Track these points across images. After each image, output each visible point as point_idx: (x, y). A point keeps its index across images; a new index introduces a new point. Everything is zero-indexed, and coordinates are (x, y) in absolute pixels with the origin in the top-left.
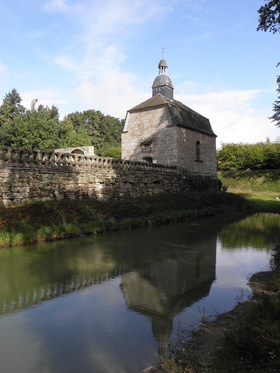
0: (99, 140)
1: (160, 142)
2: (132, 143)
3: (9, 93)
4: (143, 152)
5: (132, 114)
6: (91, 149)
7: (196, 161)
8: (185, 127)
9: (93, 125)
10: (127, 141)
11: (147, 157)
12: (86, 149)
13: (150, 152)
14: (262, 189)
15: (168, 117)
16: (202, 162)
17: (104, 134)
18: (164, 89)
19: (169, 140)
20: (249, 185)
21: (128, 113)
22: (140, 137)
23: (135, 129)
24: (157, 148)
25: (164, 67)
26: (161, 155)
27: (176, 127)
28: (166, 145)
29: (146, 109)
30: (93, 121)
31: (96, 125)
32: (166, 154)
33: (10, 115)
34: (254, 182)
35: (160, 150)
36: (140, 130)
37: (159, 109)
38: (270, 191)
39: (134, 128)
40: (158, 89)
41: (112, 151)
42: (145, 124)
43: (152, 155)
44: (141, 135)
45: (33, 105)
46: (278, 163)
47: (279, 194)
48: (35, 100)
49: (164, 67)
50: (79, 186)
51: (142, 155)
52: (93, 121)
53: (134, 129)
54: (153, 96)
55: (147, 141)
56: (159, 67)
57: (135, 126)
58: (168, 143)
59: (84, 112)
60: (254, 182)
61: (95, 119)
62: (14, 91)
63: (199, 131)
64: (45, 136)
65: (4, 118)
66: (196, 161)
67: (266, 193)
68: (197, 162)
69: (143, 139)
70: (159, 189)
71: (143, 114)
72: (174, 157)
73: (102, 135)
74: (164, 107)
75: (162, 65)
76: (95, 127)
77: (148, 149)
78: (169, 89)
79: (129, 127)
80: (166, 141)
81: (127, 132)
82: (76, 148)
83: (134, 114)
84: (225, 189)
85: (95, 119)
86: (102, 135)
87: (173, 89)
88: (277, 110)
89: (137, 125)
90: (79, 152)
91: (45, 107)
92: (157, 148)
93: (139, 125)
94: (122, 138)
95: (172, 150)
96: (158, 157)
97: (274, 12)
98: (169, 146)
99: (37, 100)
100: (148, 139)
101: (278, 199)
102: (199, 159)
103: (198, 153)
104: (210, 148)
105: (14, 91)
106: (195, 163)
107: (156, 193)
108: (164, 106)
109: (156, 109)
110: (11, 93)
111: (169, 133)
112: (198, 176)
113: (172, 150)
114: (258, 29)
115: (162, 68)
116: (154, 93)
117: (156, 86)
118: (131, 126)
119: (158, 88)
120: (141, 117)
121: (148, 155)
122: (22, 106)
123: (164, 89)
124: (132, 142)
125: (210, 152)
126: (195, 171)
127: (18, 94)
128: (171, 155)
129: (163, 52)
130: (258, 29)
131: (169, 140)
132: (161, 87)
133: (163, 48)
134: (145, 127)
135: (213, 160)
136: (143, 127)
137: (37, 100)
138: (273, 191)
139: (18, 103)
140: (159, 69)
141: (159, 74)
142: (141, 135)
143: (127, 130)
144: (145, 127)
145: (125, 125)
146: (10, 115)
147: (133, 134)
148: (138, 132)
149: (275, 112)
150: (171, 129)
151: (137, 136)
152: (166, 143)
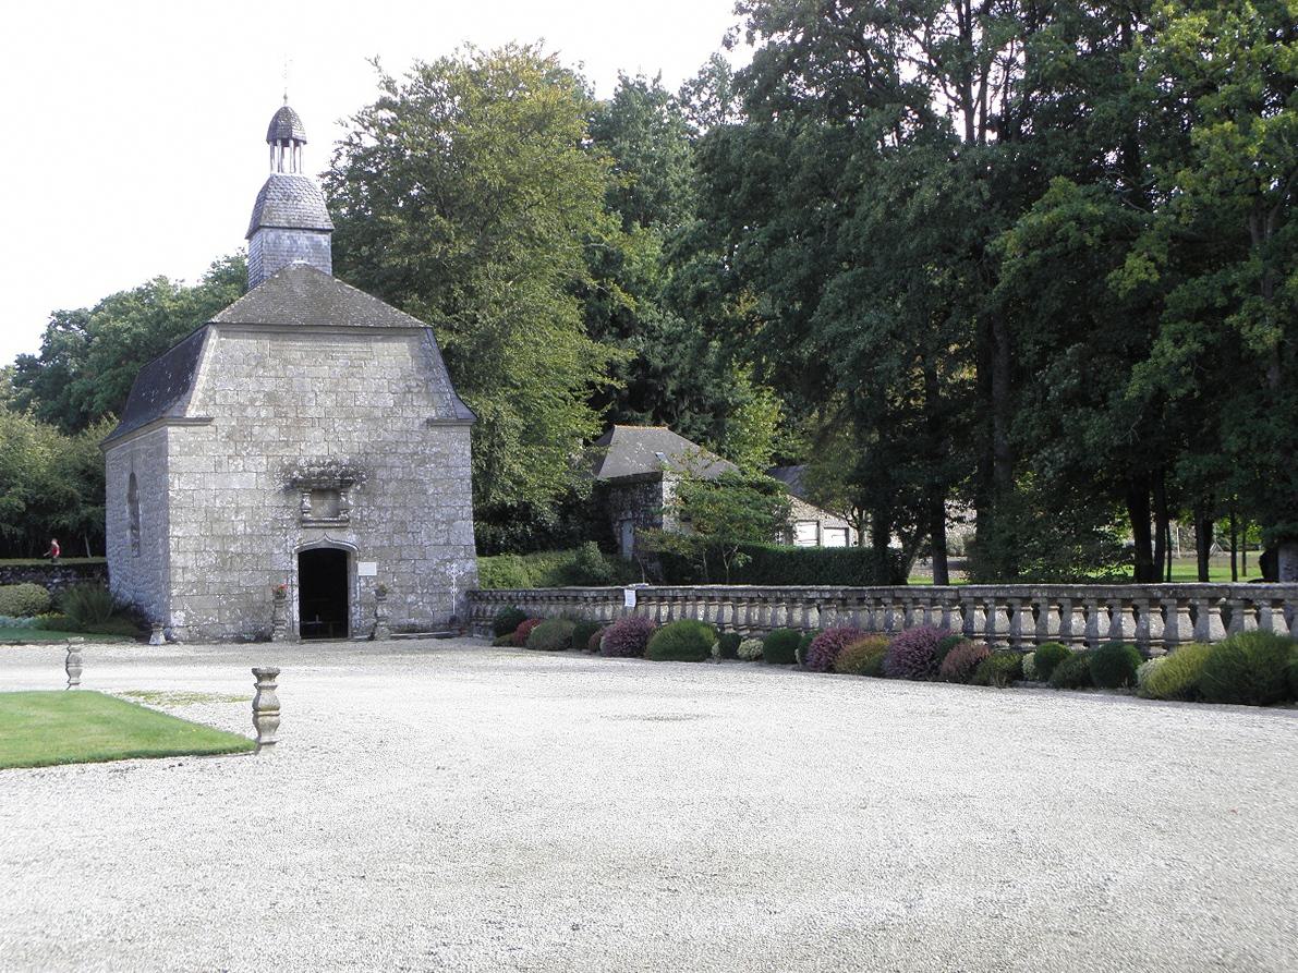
43: (349, 539)
55: (322, 473)
100: (330, 464)
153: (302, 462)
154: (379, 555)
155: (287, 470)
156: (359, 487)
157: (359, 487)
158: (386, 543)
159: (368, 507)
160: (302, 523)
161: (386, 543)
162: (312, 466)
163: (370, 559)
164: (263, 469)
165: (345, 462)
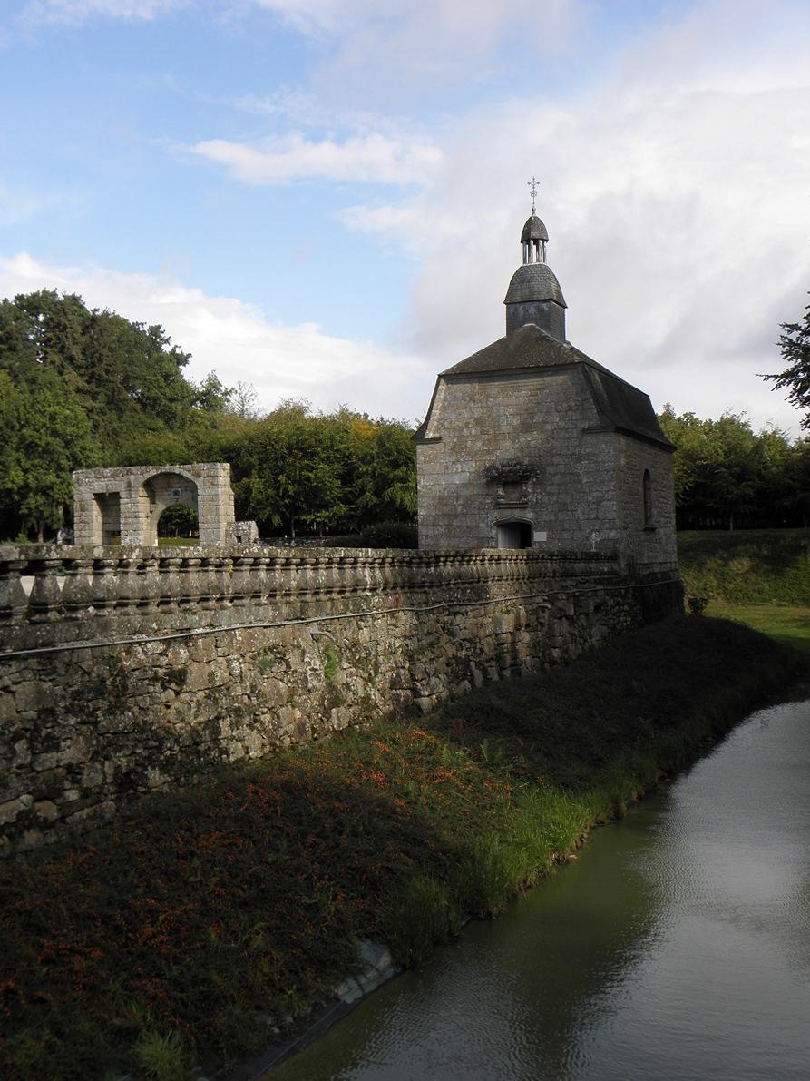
0: (87, 404)
1: (558, 476)
2: (456, 477)
4: (499, 504)
5: (456, 386)
6: (223, 473)
8: (624, 429)
9: (62, 350)
10: (439, 468)
11: (512, 520)
12: (204, 473)
13: (524, 506)
14: (757, 595)
15: (586, 405)
17: (100, 382)
19: (587, 473)
20: (712, 582)
21: (442, 381)
22: (487, 460)
24: (549, 494)
26: (560, 516)
27: (612, 434)
28: (579, 486)
29: (509, 372)
30: (62, 335)
31: (75, 351)
32: (579, 514)
34: (727, 573)
35: (556, 502)
37: (552, 375)
38: (783, 603)
39: (461, 429)
41: (150, 451)
42: (504, 418)
43: (529, 516)
44: (488, 452)
46: (729, 496)
47: (806, 612)
50: (501, 641)
52: (62, 335)
53: (462, 431)
55: (510, 471)
58: (585, 481)
59: (19, 298)
60: (727, 573)
61: (65, 327)
67: (771, 608)
70: (601, 627)
71: (494, 387)
72: (607, 526)
73: (93, 385)
74: (569, 372)
75: (534, 234)
76: (71, 359)
77: (514, 495)
79: (443, 425)
80: (578, 475)
81: (437, 440)
82: (167, 468)
83: (461, 386)
84: (697, 605)
85: (65, 327)
86: (93, 385)
87: (565, 307)
88: (796, 356)
89: (472, 421)
90: (171, 480)
92: (549, 494)
93: (479, 422)
94: (421, 458)
95: (598, 502)
96: (551, 521)
98: (591, 491)
100: (515, 465)
101: (804, 633)
103: (647, 508)
104: (664, 487)
108: (571, 369)
111: (587, 450)
113: (598, 502)
118: (450, 423)
119: (526, 305)
120: (488, 396)
121: (517, 514)
123: (547, 309)
124: (456, 473)
128: (597, 518)
129: (533, 194)
131: (587, 473)
132: (536, 304)
133: (534, 183)
134: (504, 429)
138: (792, 601)
141: (525, 261)
142: (488, 452)
143: (437, 435)
144: (504, 429)
147: (458, 449)
149: (792, 364)
150: (594, 440)
151: (474, 455)
152: (580, 482)
153: (498, 464)
154: (548, 527)
155: (488, 470)
156: (535, 480)
157: (535, 480)
158: (553, 518)
159: (541, 493)
160: (498, 505)
161: (553, 518)
162: (504, 466)
163: (542, 529)
164: (473, 470)
165: (526, 462)
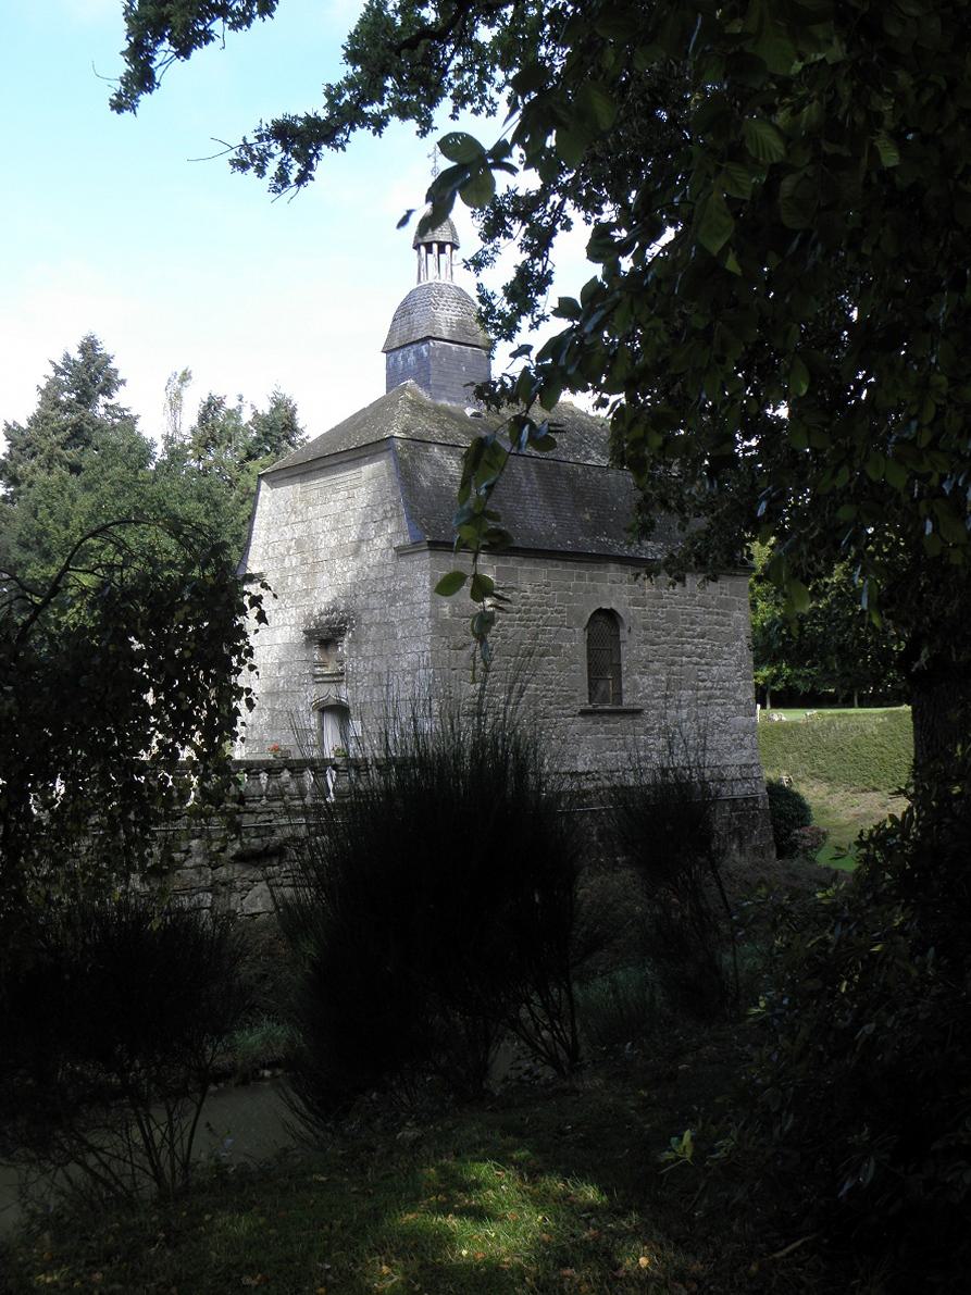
3: (67, 357)
7: (584, 713)
16: (639, 712)
18: (426, 354)
19: (403, 621)
23: (287, 564)
25: (435, 246)
27: (427, 554)
33: (71, 454)
36: (306, 568)
40: (405, 359)
43: (345, 694)
45: (175, 403)
48: (180, 374)
49: (435, 246)
51: (313, 693)
54: (389, 389)
56: (417, 247)
57: (289, 549)
62: (88, 347)
63: (602, 558)
64: (169, 553)
65: (34, 471)
66: (584, 713)
68: (596, 717)
69: (316, 612)
78: (462, 352)
89: (293, 543)
91: (231, 404)
93: (299, 543)
97: (405, 62)
99: (185, 377)
102: (620, 703)
105: (88, 347)
106: (579, 724)
107: (254, 910)
109: (359, 466)
110: (78, 357)
112: (598, 789)
114: (436, 128)
115: (429, 250)
116: (394, 377)
117: (396, 344)
120: (308, 504)
122: (121, 410)
123: (426, 354)
125: (701, 656)
126: (581, 768)
127: (108, 360)
130: (436, 128)
135: (726, 697)
136: (316, 551)
137: (185, 377)
139: (103, 399)
140: (416, 252)
145: (254, 542)
146: (71, 454)
148: (299, 580)
